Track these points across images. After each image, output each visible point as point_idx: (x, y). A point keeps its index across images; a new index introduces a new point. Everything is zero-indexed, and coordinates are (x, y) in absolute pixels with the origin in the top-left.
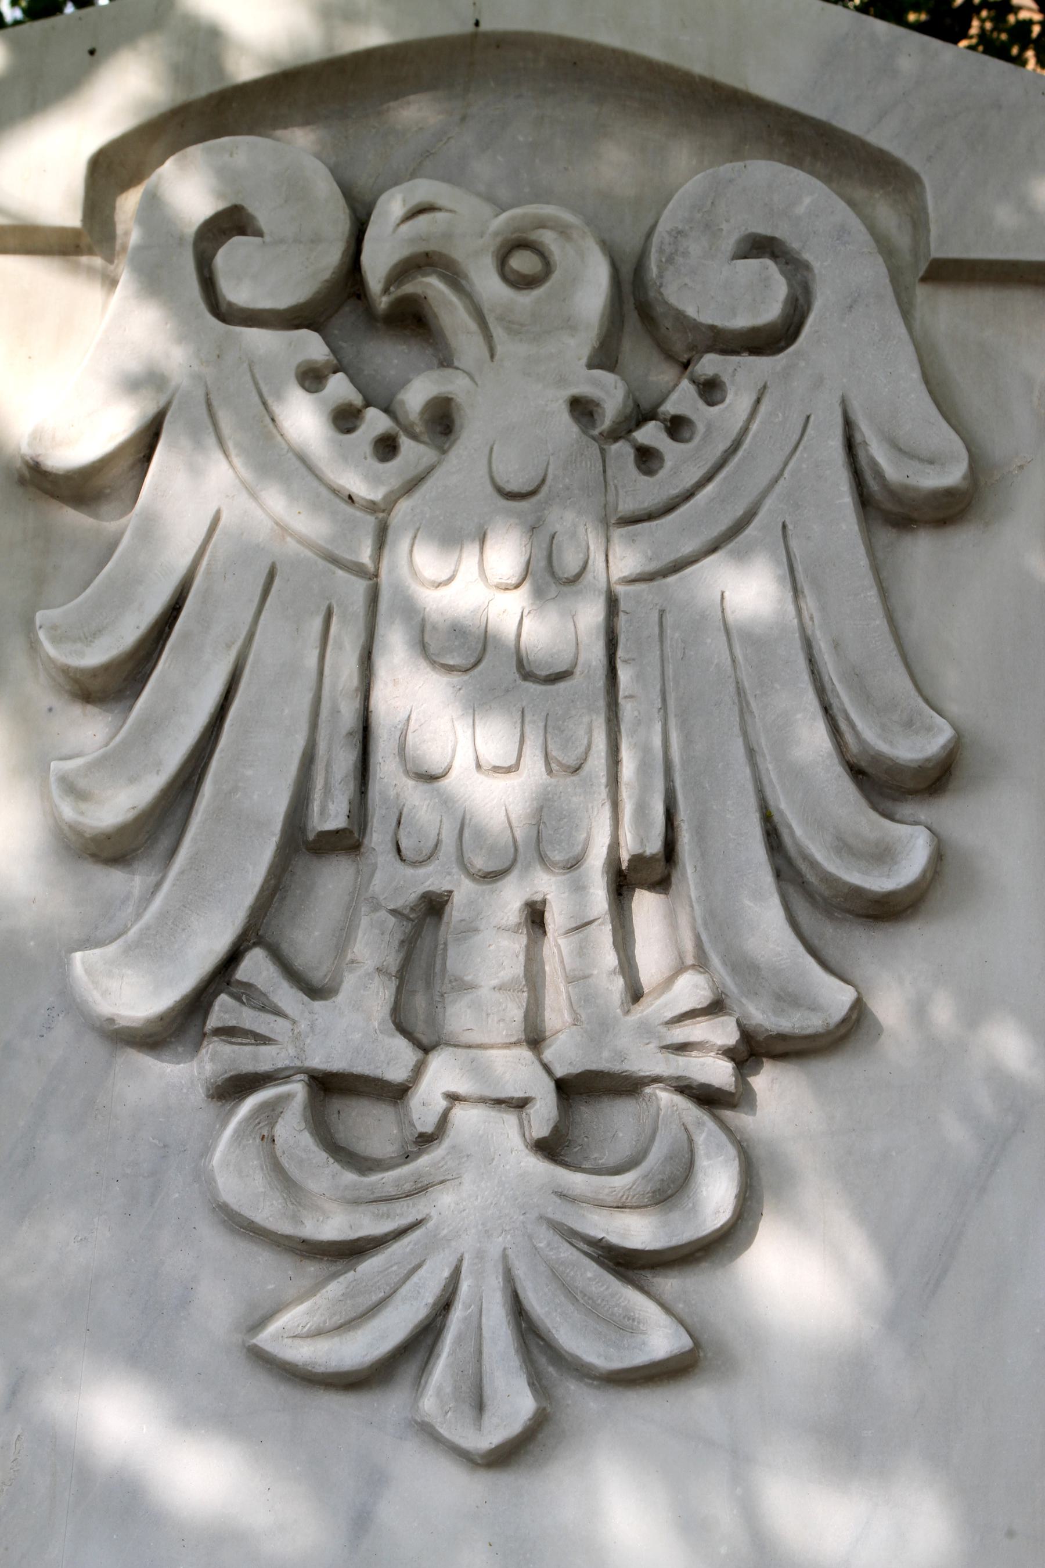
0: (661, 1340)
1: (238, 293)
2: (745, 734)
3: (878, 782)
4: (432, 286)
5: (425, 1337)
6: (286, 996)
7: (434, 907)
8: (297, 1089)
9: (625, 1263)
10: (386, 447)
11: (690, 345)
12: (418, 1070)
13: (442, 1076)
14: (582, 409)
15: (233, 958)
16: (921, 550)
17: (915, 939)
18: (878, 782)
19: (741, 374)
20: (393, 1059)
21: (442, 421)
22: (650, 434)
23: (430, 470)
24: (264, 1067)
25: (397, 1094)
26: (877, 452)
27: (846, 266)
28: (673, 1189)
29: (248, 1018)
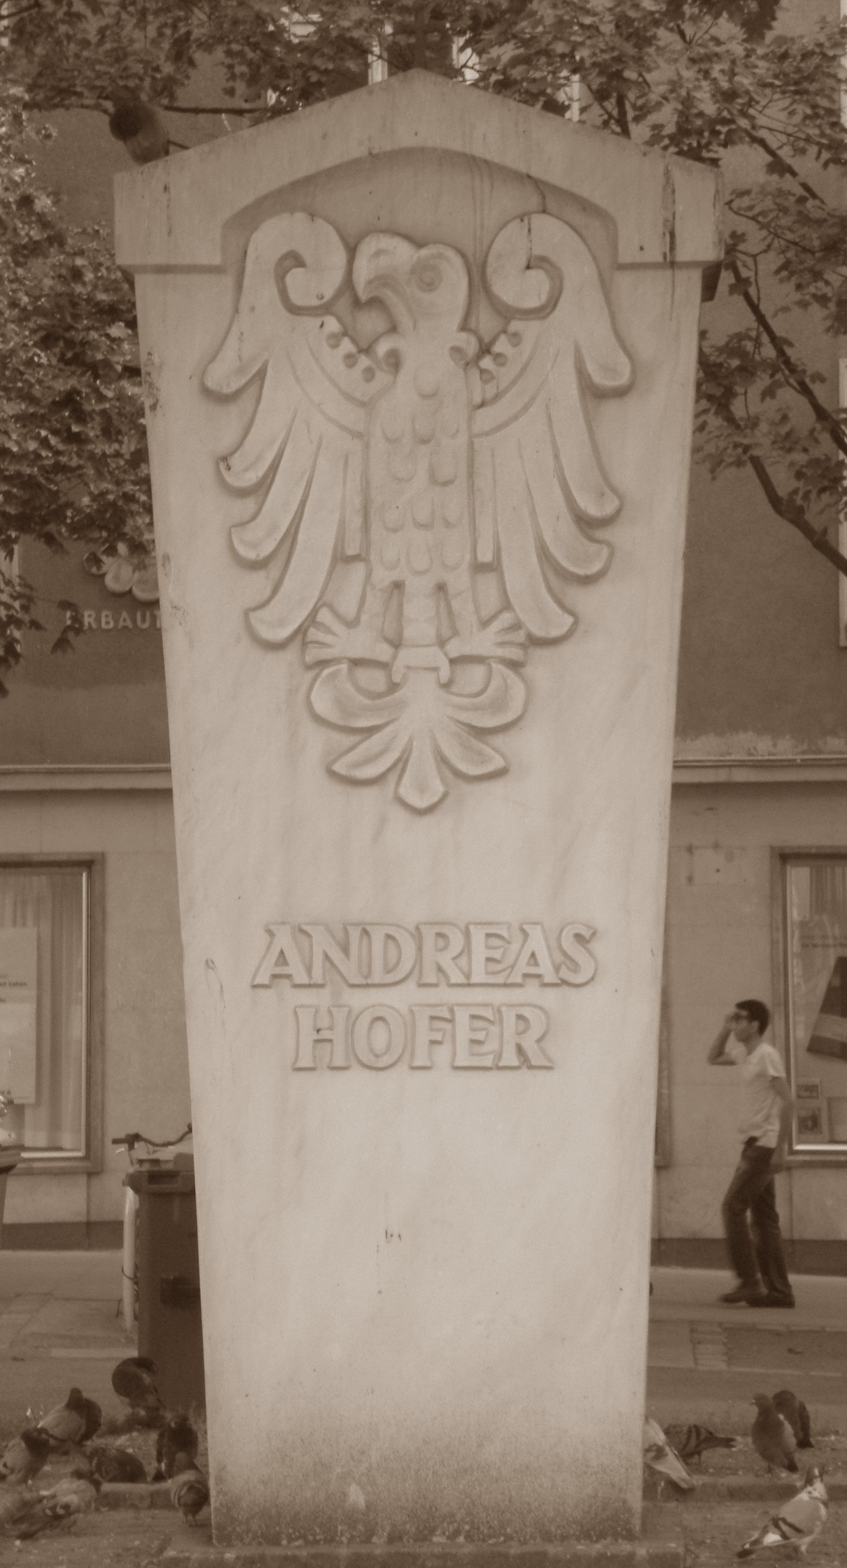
0: (498, 763)
1: (296, 298)
2: (390, 1031)
3: (588, 525)
4: (388, 295)
5: (401, 764)
6: (337, 627)
7: (398, 586)
8: (344, 667)
9: (481, 733)
10: (369, 374)
11: (507, 314)
12: (394, 657)
13: (405, 657)
14: (456, 351)
15: (315, 612)
16: (611, 409)
17: (604, 588)
18: (588, 525)
19: (530, 329)
20: (384, 652)
21: (395, 361)
22: (487, 363)
23: (425, 924)
24: (329, 657)
25: (385, 666)
26: (591, 368)
27: (579, 270)
28: (499, 704)
29: (321, 636)
